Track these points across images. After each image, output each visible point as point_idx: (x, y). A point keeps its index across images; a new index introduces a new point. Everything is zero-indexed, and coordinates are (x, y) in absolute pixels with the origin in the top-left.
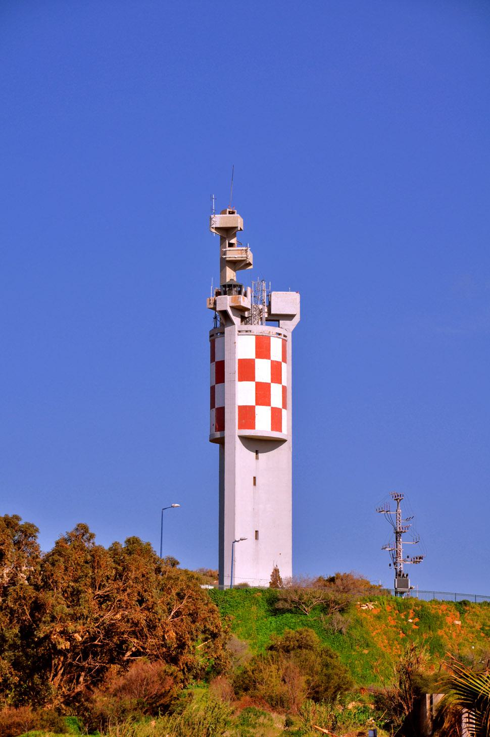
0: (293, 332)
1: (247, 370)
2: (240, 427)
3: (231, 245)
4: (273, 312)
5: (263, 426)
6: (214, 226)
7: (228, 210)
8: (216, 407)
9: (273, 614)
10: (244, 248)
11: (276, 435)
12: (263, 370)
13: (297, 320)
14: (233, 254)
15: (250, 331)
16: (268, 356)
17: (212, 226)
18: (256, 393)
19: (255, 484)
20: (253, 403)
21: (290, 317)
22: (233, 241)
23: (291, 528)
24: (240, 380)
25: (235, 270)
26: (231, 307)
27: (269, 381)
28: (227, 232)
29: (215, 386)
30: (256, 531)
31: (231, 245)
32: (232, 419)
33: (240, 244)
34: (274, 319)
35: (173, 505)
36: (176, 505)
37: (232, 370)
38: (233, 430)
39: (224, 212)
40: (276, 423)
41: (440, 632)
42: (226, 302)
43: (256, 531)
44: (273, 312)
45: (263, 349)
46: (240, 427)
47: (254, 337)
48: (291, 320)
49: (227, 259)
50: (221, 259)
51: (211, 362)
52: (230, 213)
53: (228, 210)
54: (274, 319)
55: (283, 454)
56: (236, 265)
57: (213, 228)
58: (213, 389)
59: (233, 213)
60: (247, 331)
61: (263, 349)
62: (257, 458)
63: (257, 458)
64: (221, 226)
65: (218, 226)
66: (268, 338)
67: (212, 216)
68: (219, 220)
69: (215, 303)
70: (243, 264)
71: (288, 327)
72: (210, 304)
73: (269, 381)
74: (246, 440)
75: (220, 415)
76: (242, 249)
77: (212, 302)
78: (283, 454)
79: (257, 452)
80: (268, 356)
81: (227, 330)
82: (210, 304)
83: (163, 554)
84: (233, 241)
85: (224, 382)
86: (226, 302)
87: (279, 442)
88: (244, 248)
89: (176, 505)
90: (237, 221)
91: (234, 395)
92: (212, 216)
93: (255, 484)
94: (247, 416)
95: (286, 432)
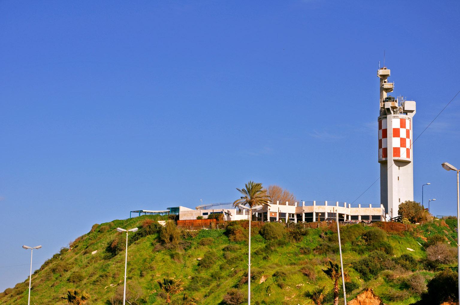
0: (413, 118)
1: (396, 133)
2: (394, 156)
3: (385, 82)
4: (405, 109)
5: (403, 156)
6: (379, 74)
7: (384, 68)
8: (383, 147)
9: (112, 246)
10: (391, 83)
11: (408, 159)
12: (403, 133)
13: (414, 112)
14: (387, 85)
15: (398, 117)
16: (405, 127)
17: (379, 74)
18: (401, 142)
19: (398, 180)
20: (400, 147)
21: (412, 111)
22: (386, 80)
23: (413, 198)
24: (394, 136)
25: (386, 93)
26: (391, 107)
27: (405, 137)
28: (384, 77)
29: (382, 139)
30: (399, 199)
31: (385, 82)
32: (390, 153)
33: (388, 82)
34: (406, 112)
35: (427, 184)
36: (429, 184)
37: (390, 133)
38: (391, 158)
39: (382, 69)
40: (408, 156)
41: (297, 251)
42: (389, 105)
43: (399, 199)
44: (405, 109)
45: (403, 124)
46: (394, 156)
47: (399, 120)
48: (412, 113)
49: (384, 88)
50: (380, 88)
51: (386, 130)
52: (385, 69)
53: (384, 68)
54: (406, 112)
55: (410, 167)
56: (387, 90)
57: (379, 75)
58: (380, 142)
59: (386, 69)
60: (394, 117)
61: (403, 124)
62: (399, 169)
63: (399, 169)
64: (382, 74)
65: (381, 74)
66: (405, 120)
67: (378, 70)
68: (381, 72)
69: (384, 105)
70: (391, 90)
71: (411, 115)
72: (382, 105)
73: (405, 137)
74: (395, 161)
75: (385, 152)
76: (390, 83)
77: (383, 105)
78: (410, 167)
79: (399, 167)
80: (405, 127)
81: (388, 116)
82: (382, 105)
83: (131, 216)
84: (386, 80)
85: (387, 137)
86: (389, 105)
87: (408, 162)
88: (391, 83)
89: (429, 184)
90: (387, 72)
91: (391, 143)
92: (378, 70)
93: (398, 180)
94: (397, 151)
95: (411, 159)
